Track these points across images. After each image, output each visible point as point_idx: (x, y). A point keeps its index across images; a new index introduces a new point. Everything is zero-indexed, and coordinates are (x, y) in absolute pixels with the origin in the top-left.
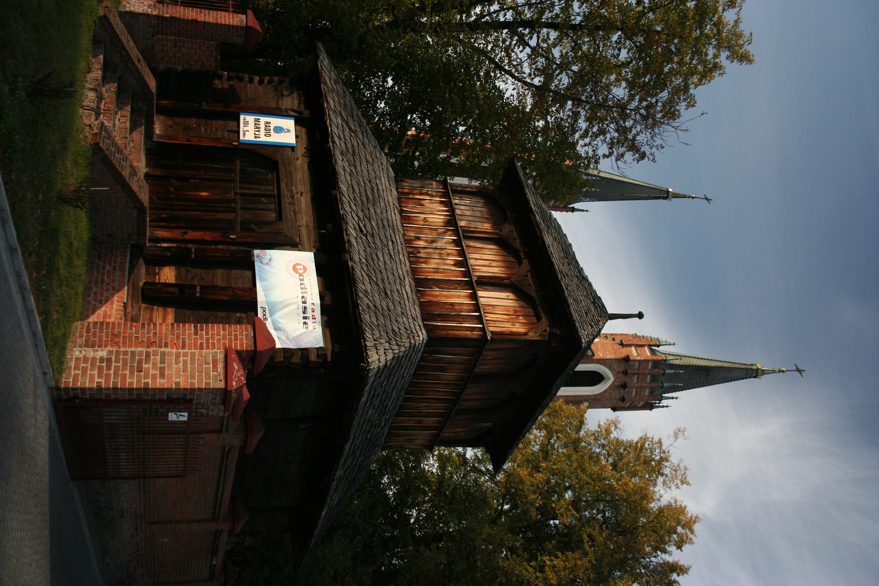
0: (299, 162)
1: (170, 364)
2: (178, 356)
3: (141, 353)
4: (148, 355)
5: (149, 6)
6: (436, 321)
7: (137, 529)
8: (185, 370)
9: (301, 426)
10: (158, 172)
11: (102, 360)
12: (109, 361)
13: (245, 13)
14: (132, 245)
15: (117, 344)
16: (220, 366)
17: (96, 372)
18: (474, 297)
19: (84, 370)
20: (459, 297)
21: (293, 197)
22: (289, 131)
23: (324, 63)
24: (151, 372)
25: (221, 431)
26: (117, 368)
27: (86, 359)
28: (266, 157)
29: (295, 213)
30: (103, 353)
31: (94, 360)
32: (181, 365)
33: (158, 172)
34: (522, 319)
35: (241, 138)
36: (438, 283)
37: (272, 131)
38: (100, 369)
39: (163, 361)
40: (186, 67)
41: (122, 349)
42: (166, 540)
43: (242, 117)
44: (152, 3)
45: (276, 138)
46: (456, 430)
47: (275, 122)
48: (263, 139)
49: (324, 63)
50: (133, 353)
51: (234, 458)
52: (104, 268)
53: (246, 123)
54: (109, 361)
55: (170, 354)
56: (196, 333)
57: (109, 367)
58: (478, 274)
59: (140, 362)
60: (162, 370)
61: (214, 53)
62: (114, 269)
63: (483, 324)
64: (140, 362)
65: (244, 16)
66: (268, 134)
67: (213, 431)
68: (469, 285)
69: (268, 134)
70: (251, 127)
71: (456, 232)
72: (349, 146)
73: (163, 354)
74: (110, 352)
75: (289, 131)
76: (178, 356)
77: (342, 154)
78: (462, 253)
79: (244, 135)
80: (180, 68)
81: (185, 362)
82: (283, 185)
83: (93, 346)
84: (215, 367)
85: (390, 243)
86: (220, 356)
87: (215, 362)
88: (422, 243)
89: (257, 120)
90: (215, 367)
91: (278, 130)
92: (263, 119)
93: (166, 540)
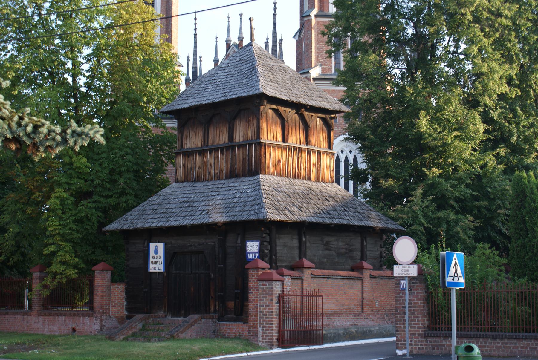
0: (173, 242)
1: (264, 303)
2: (261, 300)
3: (260, 315)
4: (261, 312)
5: (96, 320)
6: (252, 170)
7: (367, 318)
8: (266, 297)
9: (304, 239)
10: (183, 312)
11: (262, 330)
12: (263, 327)
13: (94, 271)
14: (218, 321)
15: (257, 324)
16: (264, 282)
17: (267, 332)
18: (239, 146)
19: (266, 336)
20: (239, 154)
21: (191, 246)
22: (156, 246)
23: (114, 226)
24: (267, 310)
25: (302, 279)
26: (266, 324)
27: (262, 336)
28: (170, 258)
29: (199, 245)
30: (260, 329)
31: (263, 333)
32: (264, 299)
33: (183, 312)
34: (251, 118)
35: (162, 271)
36: (233, 165)
37: (157, 255)
38: (266, 330)
39: (263, 306)
40: (124, 300)
41: (259, 322)
42: (377, 304)
43: (151, 271)
44: (94, 319)
45: (161, 253)
46: (321, 140)
47: (152, 253)
48: (162, 260)
49: (114, 226)
50: (260, 318)
51: (319, 272)
52: (229, 333)
53: (154, 268)
54: (263, 327)
55: (260, 303)
56: (252, 293)
57: (265, 327)
58: (227, 140)
59: (263, 315)
60: (266, 306)
61: (116, 286)
62: (229, 328)
63: (253, 144)
64: (263, 315)
65: (96, 272)
66: (159, 257)
67: (302, 283)
68: (233, 148)
69: (159, 257)
70: (156, 266)
71: (205, 151)
72: (162, 215)
73: (260, 306)
74: (260, 326)
75: (156, 246)
76: (261, 300)
77: (168, 221)
78: (216, 150)
79: (160, 269)
80: (125, 303)
81: (263, 297)
82: (186, 250)
83: (257, 333)
84: (265, 285)
85: (223, 87)
86: (261, 283)
87: (263, 285)
88: (212, 171)
89: (152, 263)
90: (265, 285)
91: (156, 252)
92: (151, 260)
93: (377, 304)
